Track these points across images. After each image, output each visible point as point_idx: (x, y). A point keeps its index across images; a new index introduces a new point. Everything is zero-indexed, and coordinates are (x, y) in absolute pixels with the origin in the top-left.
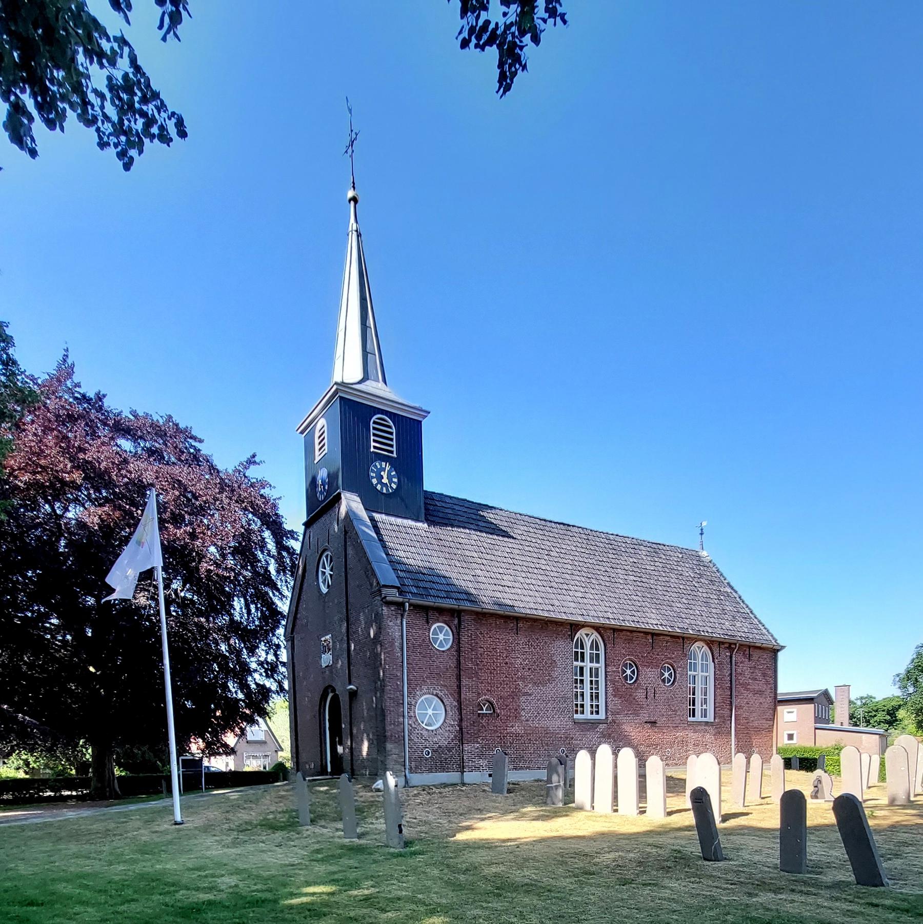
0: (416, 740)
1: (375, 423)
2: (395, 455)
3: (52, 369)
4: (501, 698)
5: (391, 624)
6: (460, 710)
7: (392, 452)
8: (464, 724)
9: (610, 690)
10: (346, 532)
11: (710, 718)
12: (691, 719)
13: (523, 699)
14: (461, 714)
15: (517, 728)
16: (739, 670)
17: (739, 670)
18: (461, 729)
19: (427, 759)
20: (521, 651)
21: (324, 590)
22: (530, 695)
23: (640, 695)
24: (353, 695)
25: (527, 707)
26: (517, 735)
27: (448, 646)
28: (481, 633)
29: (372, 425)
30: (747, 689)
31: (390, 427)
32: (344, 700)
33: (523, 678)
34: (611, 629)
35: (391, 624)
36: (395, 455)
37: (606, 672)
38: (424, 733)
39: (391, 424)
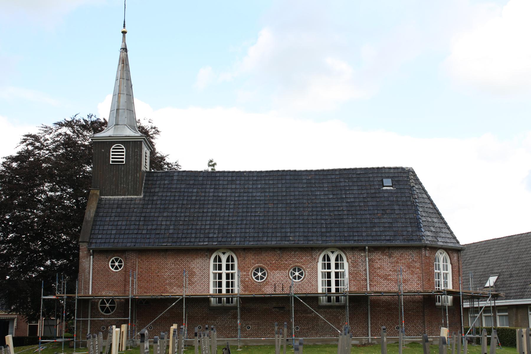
1: (113, 149)
7: (123, 162)
28: (141, 260)
29: (111, 150)
30: (388, 280)
33: (170, 284)
39: (123, 147)
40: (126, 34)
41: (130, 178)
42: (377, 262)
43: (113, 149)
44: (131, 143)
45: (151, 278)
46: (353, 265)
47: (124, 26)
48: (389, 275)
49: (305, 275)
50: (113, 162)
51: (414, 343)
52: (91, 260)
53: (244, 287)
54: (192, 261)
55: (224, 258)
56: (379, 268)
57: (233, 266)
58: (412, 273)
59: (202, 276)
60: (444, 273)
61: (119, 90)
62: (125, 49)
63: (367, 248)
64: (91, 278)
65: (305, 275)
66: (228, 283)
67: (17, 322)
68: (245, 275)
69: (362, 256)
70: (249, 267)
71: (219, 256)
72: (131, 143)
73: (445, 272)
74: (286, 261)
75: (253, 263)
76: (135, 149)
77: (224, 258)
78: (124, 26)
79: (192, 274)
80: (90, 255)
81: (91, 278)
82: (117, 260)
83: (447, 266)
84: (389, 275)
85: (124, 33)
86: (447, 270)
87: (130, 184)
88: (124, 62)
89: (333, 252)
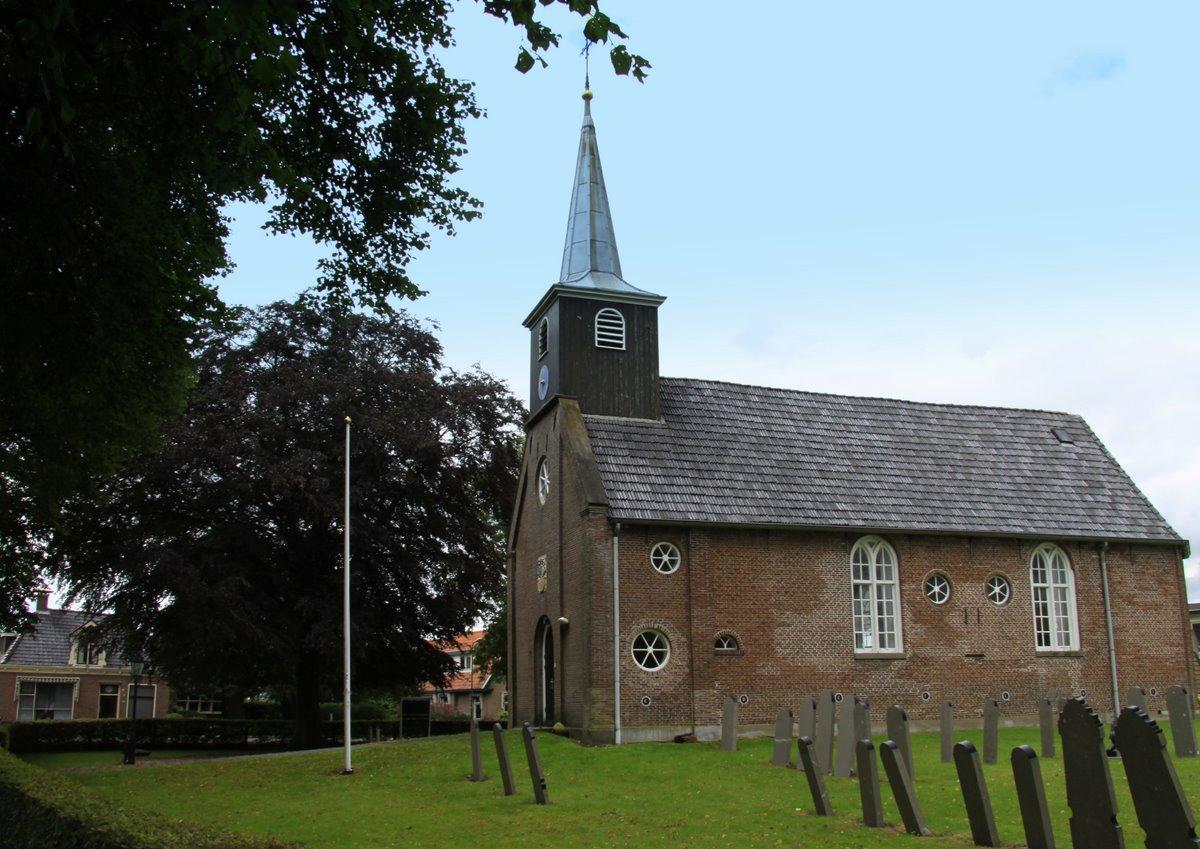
0: (631, 684)
1: (600, 317)
2: (624, 348)
3: (413, 280)
4: (747, 630)
5: (599, 546)
6: (690, 647)
7: (621, 345)
8: (696, 664)
9: (909, 615)
10: (561, 442)
11: (1075, 645)
12: (1043, 649)
13: (778, 630)
14: (691, 652)
15: (769, 669)
16: (1117, 578)
17: (1117, 578)
18: (692, 671)
19: (645, 710)
20: (774, 570)
21: (543, 502)
22: (789, 625)
23: (955, 620)
24: (565, 628)
25: (785, 640)
26: (771, 678)
27: (676, 569)
28: (718, 551)
29: (597, 319)
30: (1134, 604)
31: (619, 319)
32: (556, 633)
33: (778, 605)
34: (905, 535)
35: (599, 546)
36: (624, 348)
37: (901, 591)
38: (642, 676)
39: (621, 315)
40: (591, 101)
41: (637, 379)
42: (1115, 572)
43: (600, 317)
44: (636, 308)
45: (741, 590)
46: (1081, 577)
47: (587, 86)
48: (1134, 596)
49: (1011, 592)
50: (600, 343)
51: (679, 740)
52: (616, 546)
53: (914, 615)
54: (818, 558)
55: (873, 556)
56: (1120, 582)
57: (889, 570)
58: (1166, 593)
59: (838, 589)
60: (1036, 589)
61: (592, 205)
62: (590, 128)
63: (1106, 544)
64: (617, 586)
65: (1011, 592)
66: (880, 606)
67: (80, 691)
68: (914, 590)
69: (1093, 560)
70: (920, 575)
71: (863, 551)
72: (636, 308)
73: (1040, 585)
74: (980, 564)
75: (927, 566)
76: (644, 324)
77: (873, 556)
78: (587, 86)
79: (820, 585)
80: (615, 535)
81: (617, 586)
82: (665, 549)
83: (1063, 573)
84: (1134, 596)
85: (587, 98)
86: (1063, 581)
87: (637, 393)
88: (590, 149)
89: (871, 545)
